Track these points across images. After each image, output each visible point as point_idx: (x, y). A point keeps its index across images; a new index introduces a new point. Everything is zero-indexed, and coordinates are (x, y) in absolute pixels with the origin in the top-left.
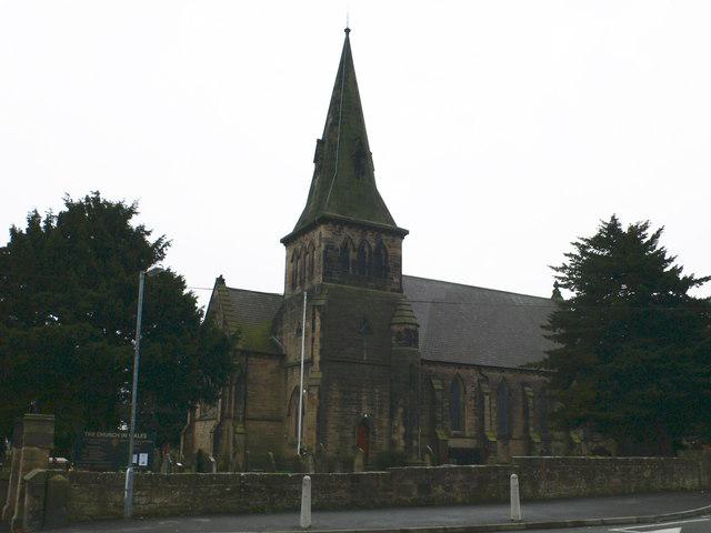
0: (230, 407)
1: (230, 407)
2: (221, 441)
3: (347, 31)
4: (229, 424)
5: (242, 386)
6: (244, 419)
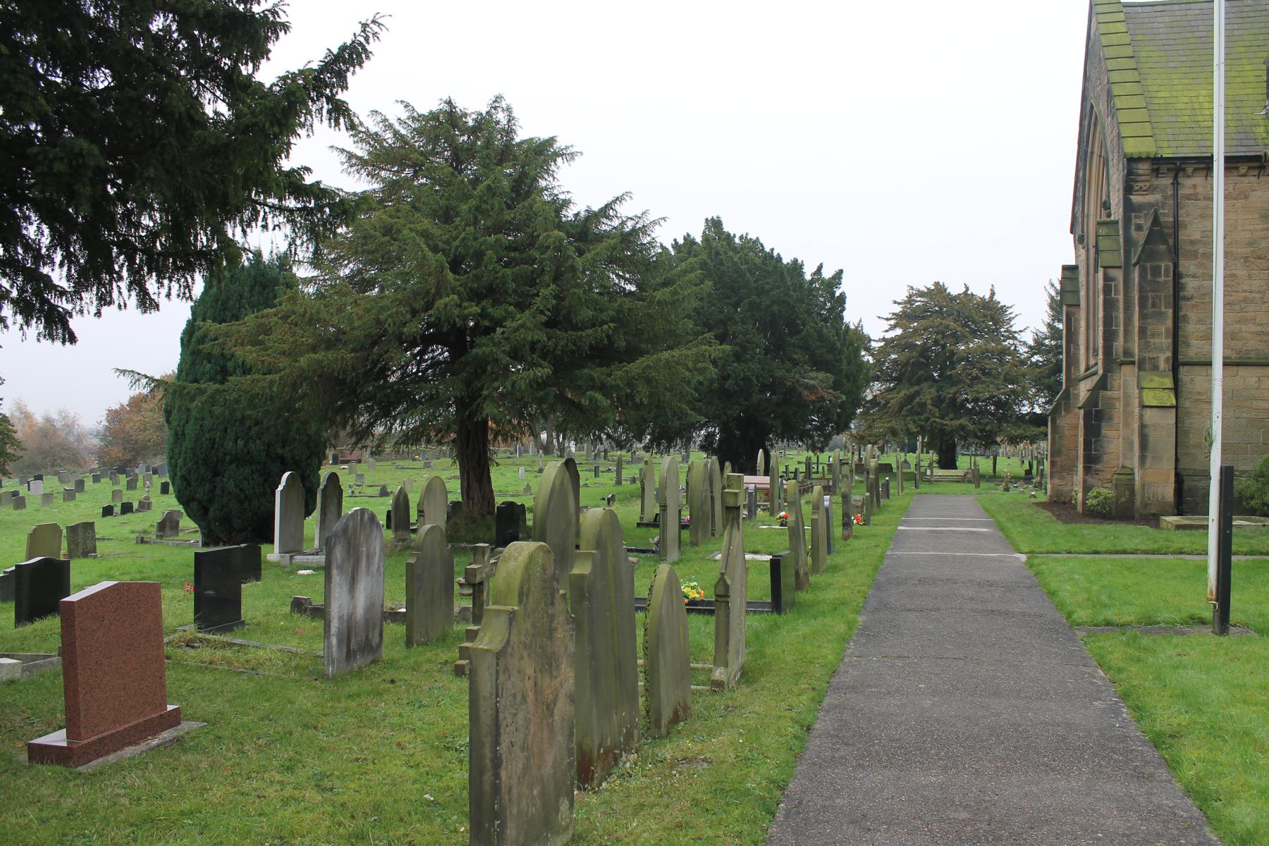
0: (1127, 333)
1: (1127, 333)
2: (1106, 431)
4: (1126, 377)
5: (1166, 264)
6: (1176, 365)
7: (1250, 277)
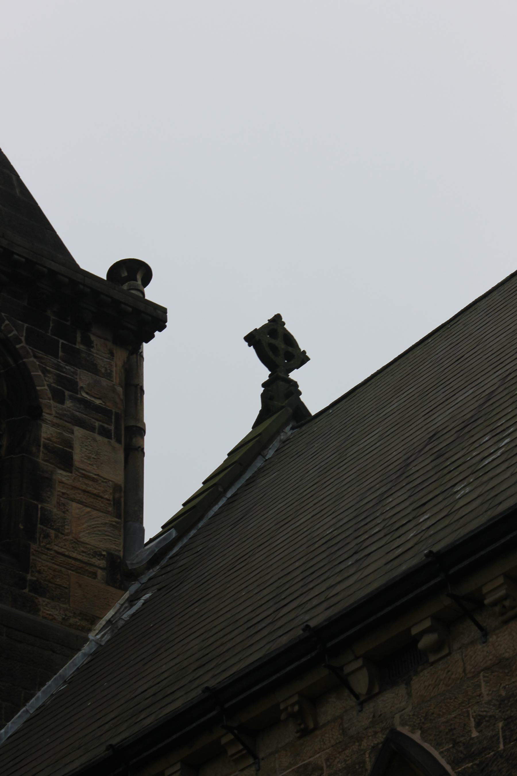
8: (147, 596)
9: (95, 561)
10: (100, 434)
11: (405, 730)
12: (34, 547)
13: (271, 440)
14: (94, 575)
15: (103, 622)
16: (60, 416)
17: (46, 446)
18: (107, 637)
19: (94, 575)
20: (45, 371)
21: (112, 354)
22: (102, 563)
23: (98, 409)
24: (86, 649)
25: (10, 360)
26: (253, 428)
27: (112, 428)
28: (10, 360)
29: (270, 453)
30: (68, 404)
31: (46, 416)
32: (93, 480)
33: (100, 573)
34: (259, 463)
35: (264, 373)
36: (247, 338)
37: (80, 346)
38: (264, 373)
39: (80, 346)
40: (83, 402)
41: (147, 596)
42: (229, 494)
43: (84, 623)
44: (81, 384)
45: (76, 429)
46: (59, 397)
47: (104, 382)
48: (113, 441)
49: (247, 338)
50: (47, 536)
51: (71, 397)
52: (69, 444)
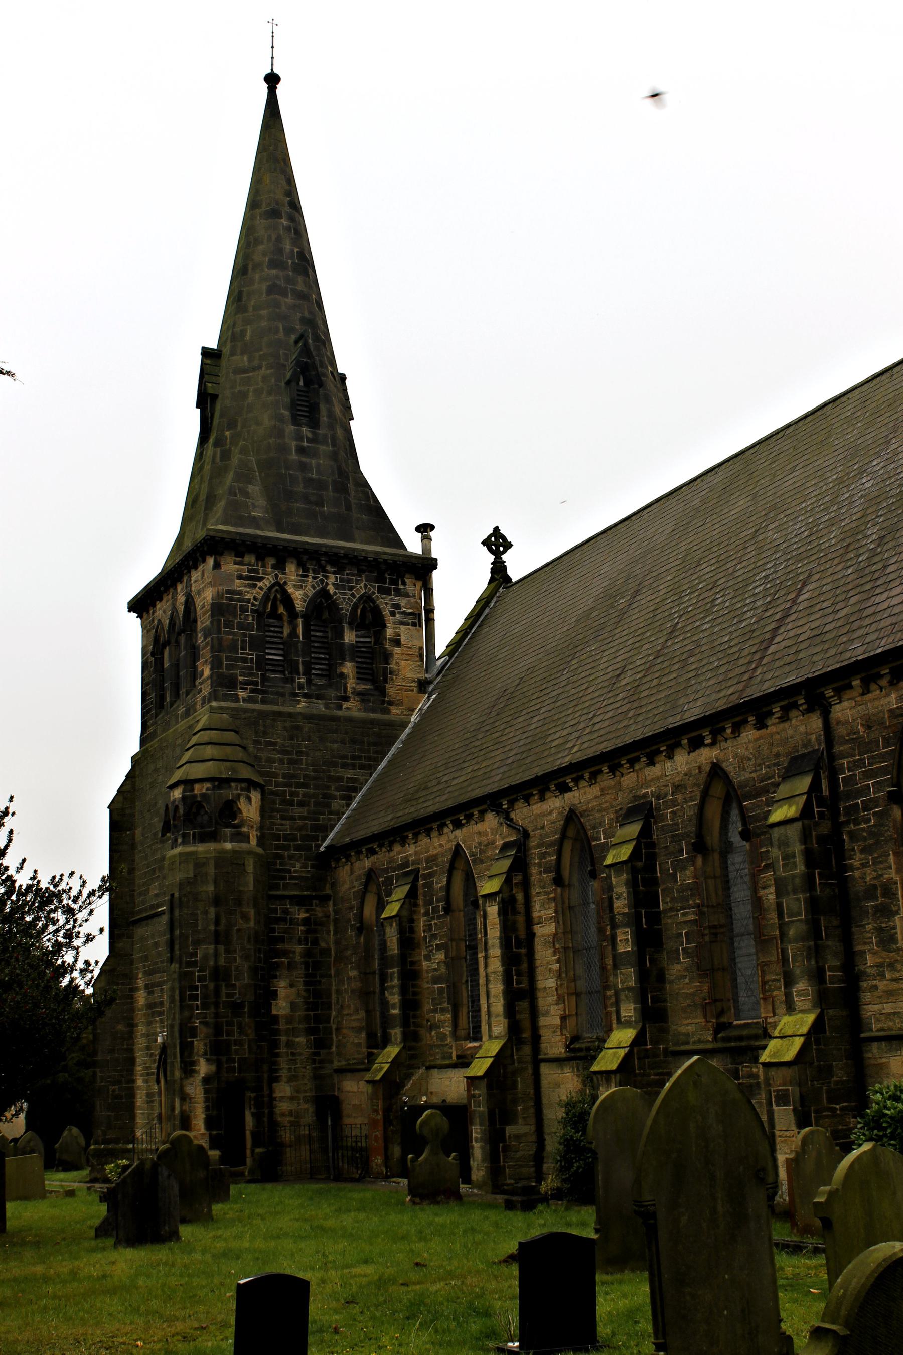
3: (272, 80)
7: (146, 958)
8: (434, 696)
9: (413, 684)
10: (412, 626)
11: (461, 843)
12: (387, 685)
13: (492, 598)
14: (413, 690)
15: (417, 710)
16: (394, 623)
17: (389, 640)
18: (418, 719)
19: (413, 690)
20: (386, 604)
21: (415, 585)
22: (416, 684)
23: (410, 614)
24: (410, 726)
25: (371, 604)
26: (488, 584)
27: (417, 621)
28: (371, 604)
29: (492, 604)
30: (397, 616)
31: (388, 625)
32: (410, 648)
33: (415, 689)
34: (487, 611)
35: (492, 558)
36: (482, 543)
37: (401, 586)
38: (492, 558)
39: (401, 586)
40: (405, 613)
41: (434, 696)
42: (472, 632)
43: (410, 712)
44: (402, 605)
45: (402, 627)
46: (393, 614)
47: (412, 600)
48: (418, 627)
49: (482, 543)
50: (392, 679)
51: (399, 613)
52: (398, 635)
